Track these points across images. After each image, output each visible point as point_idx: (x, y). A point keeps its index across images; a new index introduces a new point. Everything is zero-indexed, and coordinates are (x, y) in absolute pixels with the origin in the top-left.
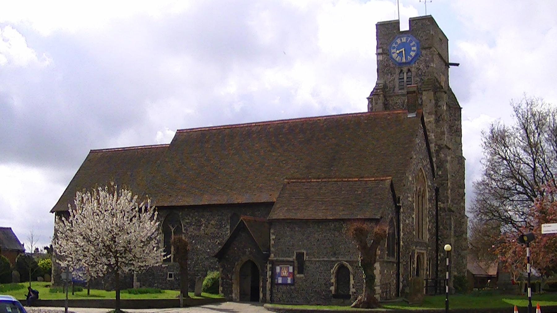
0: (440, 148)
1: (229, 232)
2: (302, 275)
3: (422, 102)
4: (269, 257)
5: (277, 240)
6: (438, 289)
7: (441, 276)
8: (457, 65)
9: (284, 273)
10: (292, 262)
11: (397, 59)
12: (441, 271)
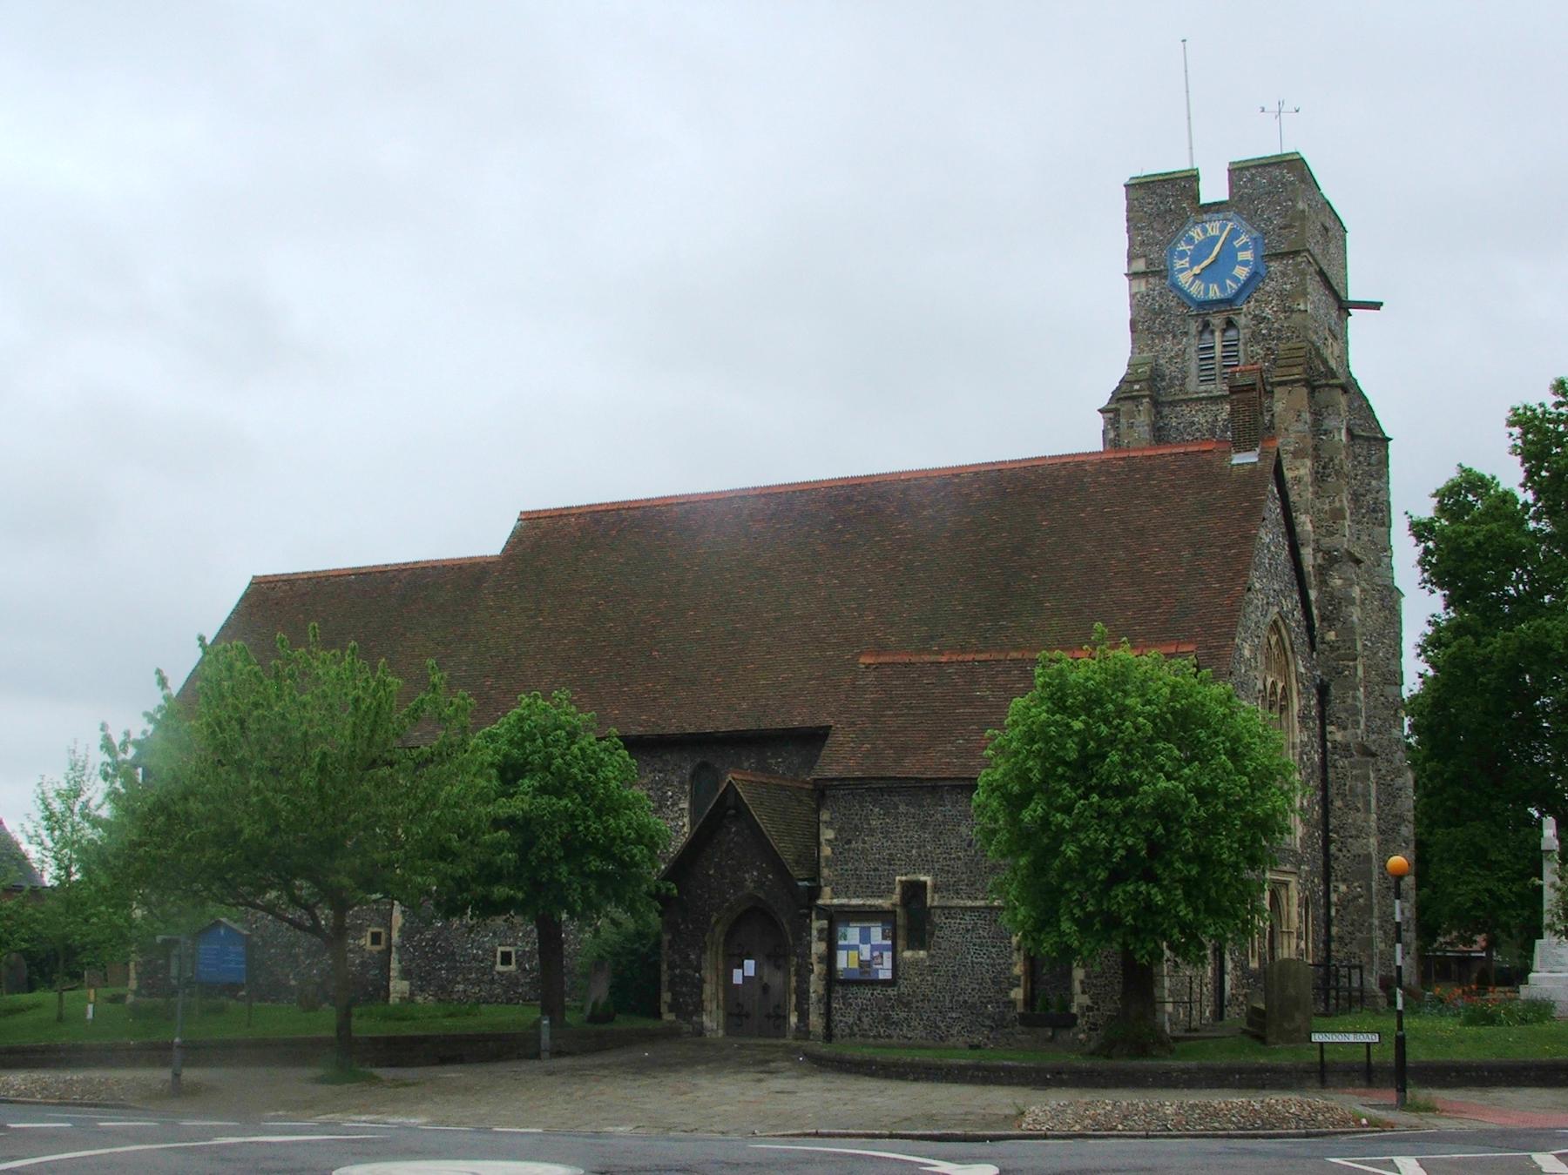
0: (1331, 560)
1: (686, 820)
2: (922, 953)
3: (1271, 422)
4: (818, 897)
5: (844, 840)
6: (1333, 993)
7: (1341, 955)
8: (1376, 306)
9: (861, 947)
10: (888, 912)
11: (1193, 291)
12: (1341, 938)
